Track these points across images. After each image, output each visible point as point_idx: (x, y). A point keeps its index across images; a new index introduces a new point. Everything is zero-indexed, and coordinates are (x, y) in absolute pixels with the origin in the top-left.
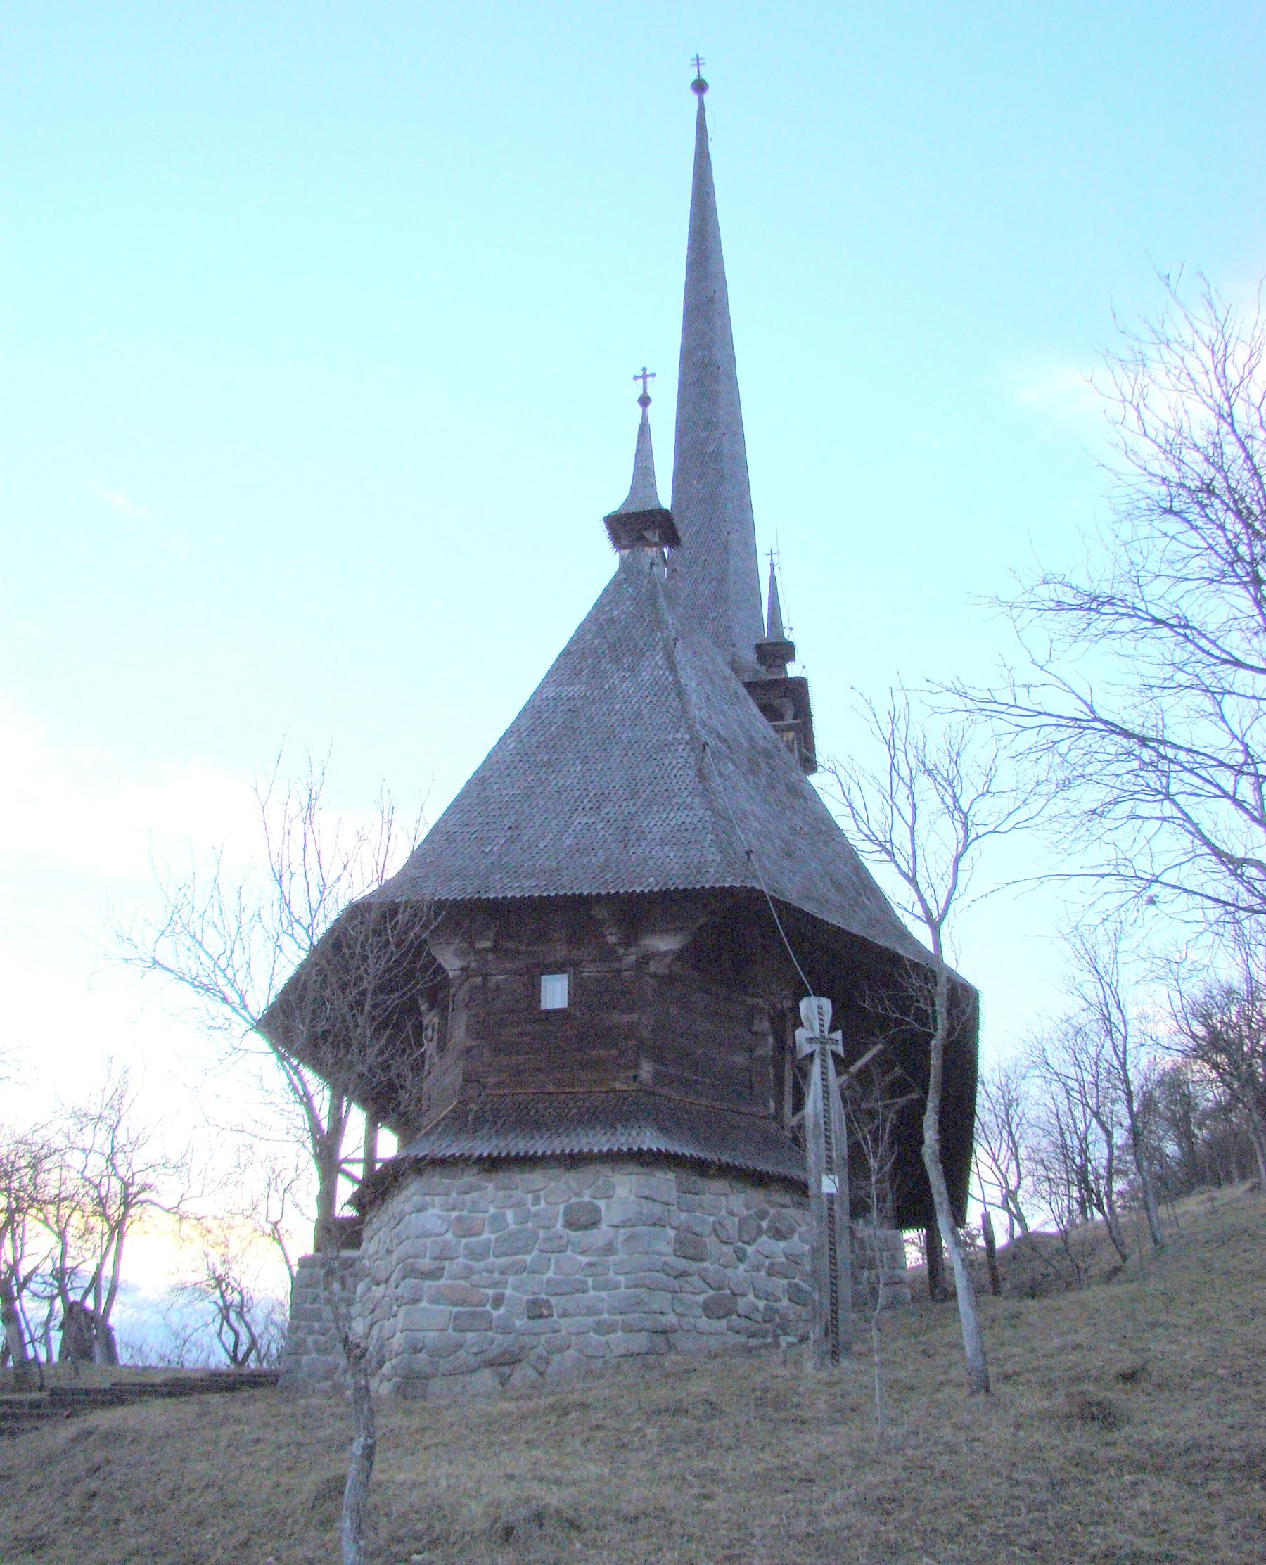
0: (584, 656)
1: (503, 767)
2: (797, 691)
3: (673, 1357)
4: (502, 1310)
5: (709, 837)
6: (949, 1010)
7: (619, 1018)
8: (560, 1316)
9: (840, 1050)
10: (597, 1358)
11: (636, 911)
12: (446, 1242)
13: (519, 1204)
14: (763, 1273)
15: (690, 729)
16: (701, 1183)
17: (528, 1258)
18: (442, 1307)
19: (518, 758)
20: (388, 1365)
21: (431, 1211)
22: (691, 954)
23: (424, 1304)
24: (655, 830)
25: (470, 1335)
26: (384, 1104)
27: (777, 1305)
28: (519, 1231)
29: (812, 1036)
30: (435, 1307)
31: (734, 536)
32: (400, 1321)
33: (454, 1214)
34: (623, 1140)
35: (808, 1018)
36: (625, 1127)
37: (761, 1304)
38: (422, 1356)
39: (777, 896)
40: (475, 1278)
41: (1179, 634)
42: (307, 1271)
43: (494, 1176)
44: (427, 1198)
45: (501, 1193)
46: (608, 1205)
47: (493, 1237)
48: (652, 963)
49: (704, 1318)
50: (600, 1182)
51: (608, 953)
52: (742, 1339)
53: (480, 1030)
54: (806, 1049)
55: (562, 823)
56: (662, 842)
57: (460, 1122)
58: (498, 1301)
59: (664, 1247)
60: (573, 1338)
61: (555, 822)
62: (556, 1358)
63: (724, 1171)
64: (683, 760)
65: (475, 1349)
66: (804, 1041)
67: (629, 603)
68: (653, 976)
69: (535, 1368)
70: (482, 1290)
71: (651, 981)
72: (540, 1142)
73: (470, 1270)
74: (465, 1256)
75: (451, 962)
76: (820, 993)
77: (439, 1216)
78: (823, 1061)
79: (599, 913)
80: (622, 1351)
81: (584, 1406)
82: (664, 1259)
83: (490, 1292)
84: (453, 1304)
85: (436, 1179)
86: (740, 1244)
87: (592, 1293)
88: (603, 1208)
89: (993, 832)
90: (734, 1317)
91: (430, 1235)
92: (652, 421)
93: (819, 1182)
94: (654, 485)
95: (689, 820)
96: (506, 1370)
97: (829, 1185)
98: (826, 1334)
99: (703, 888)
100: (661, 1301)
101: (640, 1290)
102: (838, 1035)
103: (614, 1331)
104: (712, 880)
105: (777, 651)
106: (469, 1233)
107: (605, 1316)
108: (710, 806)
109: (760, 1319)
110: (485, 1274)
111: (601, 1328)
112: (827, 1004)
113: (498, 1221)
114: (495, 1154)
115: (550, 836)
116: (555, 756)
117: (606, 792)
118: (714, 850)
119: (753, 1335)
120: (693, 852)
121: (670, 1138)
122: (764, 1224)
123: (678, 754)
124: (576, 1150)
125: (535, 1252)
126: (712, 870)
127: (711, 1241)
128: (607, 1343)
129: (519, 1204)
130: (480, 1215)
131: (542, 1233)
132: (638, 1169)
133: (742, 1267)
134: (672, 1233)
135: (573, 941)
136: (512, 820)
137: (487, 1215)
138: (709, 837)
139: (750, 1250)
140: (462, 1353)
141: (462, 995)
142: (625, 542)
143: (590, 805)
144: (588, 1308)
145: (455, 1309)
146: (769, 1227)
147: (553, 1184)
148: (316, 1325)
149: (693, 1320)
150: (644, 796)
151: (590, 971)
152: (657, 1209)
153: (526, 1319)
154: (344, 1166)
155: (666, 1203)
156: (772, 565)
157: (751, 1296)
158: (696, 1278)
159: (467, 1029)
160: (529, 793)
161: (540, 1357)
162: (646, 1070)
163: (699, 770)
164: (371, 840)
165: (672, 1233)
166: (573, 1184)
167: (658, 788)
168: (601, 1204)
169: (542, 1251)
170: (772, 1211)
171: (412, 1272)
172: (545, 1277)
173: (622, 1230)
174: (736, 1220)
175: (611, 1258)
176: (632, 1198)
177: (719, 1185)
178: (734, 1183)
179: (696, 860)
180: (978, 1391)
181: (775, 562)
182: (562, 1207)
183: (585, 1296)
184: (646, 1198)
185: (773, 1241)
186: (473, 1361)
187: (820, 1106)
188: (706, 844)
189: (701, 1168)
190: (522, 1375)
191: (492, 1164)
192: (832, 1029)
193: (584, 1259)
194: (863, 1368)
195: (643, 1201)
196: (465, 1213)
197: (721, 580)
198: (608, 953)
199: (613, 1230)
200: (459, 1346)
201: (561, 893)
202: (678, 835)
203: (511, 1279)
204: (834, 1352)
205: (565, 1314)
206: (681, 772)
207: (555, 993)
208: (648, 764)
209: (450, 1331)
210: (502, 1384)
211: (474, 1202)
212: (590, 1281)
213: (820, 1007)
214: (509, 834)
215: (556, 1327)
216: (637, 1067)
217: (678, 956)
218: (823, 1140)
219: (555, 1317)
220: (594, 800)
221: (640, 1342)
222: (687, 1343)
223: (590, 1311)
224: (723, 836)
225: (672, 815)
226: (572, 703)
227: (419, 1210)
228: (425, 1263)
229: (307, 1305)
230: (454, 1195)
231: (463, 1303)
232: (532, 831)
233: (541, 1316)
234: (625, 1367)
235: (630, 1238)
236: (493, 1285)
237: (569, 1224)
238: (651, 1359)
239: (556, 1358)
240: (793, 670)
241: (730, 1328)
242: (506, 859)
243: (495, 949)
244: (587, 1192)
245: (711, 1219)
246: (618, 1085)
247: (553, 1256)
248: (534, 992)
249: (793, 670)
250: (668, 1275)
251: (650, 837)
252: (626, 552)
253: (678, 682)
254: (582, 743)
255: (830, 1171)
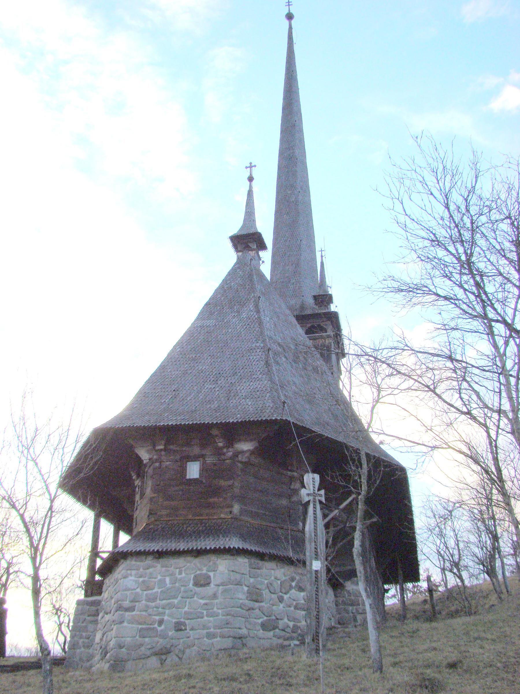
0: (216, 305)
1: (173, 360)
2: (333, 319)
3: (245, 650)
4: (163, 627)
5: (268, 395)
6: (368, 482)
7: (222, 483)
8: (190, 630)
9: (323, 500)
10: (208, 651)
11: (232, 431)
12: (136, 593)
13: (172, 574)
14: (292, 608)
15: (264, 341)
16: (261, 563)
17: (176, 601)
18: (134, 625)
19: (181, 356)
20: (108, 655)
21: (130, 578)
22: (258, 452)
23: (125, 624)
24: (243, 391)
25: (147, 639)
26: (123, 521)
27: (299, 624)
28: (172, 588)
29: (309, 492)
30: (130, 625)
31: (304, 242)
32: (113, 633)
33: (141, 579)
34: (222, 543)
35: (307, 484)
36: (223, 537)
37: (291, 624)
38: (124, 650)
39: (298, 423)
40: (150, 610)
41: (452, 303)
42: (80, 607)
43: (160, 560)
44: (129, 572)
45: (164, 569)
46: (214, 575)
47: (159, 590)
48: (239, 456)
49: (261, 631)
50: (211, 563)
51: (218, 452)
52: (280, 641)
53: (156, 490)
54: (306, 499)
55: (199, 389)
56: (245, 398)
57: (148, 534)
58: (161, 622)
59: (240, 596)
60: (196, 640)
61: (196, 387)
62: (188, 651)
63: (273, 558)
64: (259, 357)
65: (149, 647)
66: (305, 495)
67: (239, 279)
68: (241, 462)
69: (177, 656)
70: (153, 617)
71: (239, 465)
72: (183, 544)
73: (148, 606)
74: (146, 600)
75: (144, 455)
76: (314, 472)
77: (133, 581)
78: (314, 505)
79: (215, 432)
80: (219, 647)
81: (189, 676)
82: (241, 601)
83: (157, 618)
84: (140, 624)
85: (133, 562)
86: (281, 594)
87: (206, 618)
88: (212, 577)
89: (390, 394)
90: (277, 630)
91: (129, 590)
92: (254, 189)
93: (311, 564)
94: (254, 221)
95: (259, 386)
96: (164, 657)
97: (317, 565)
98: (313, 640)
99: (258, 420)
100: (239, 622)
101: (228, 617)
102: (322, 492)
103: (216, 637)
104: (267, 416)
105: (324, 299)
106: (148, 588)
107: (212, 630)
108: (271, 380)
109: (290, 631)
110: (155, 609)
111: (210, 636)
112: (317, 477)
113: (162, 582)
114: (160, 550)
115: (193, 394)
116: (198, 355)
117: (221, 372)
118: (270, 401)
119: (287, 639)
120: (260, 402)
121: (245, 542)
122: (294, 584)
123: (257, 354)
124: (199, 548)
125: (179, 598)
126: (268, 411)
127: (266, 593)
128: (213, 644)
129: (172, 574)
130: (153, 580)
131: (183, 589)
132: (229, 557)
133: (281, 605)
134: (246, 589)
135: (203, 446)
136: (176, 387)
137: (156, 580)
138: (268, 395)
139: (286, 597)
140: (143, 648)
141: (150, 471)
142: (239, 249)
143: (213, 379)
144: (204, 626)
145: (140, 626)
146: (296, 585)
147: (188, 564)
148: (84, 634)
149: (255, 632)
150: (239, 374)
151: (209, 460)
152: (238, 576)
153: (174, 632)
154: (100, 554)
155: (243, 574)
156: (322, 256)
157: (286, 620)
158: (257, 610)
159: (151, 489)
160: (185, 373)
161: (180, 650)
162: (236, 508)
163: (267, 362)
164: (109, 395)
165: (246, 589)
166: (198, 565)
167: (246, 370)
168: (211, 574)
169: (182, 598)
170: (297, 578)
171: (120, 608)
172: (184, 610)
173: (221, 587)
174: (279, 582)
175: (216, 601)
176: (226, 571)
177: (271, 565)
178: (279, 564)
179: (261, 406)
180: (376, 671)
181: (323, 255)
182: (192, 576)
183: (202, 620)
184: (233, 571)
185: (298, 592)
186: (148, 653)
187: (313, 527)
188: (267, 398)
189: (261, 556)
190: (172, 659)
191: (160, 555)
192: (319, 490)
193: (203, 602)
194: (329, 658)
195: (232, 573)
196: (146, 579)
197: (298, 265)
198: (218, 452)
199: (217, 587)
200: (142, 645)
201: (195, 423)
202: (254, 393)
203: (167, 611)
204: (317, 649)
205: (192, 629)
206: (258, 362)
207: (194, 471)
208: (242, 358)
209: (138, 637)
210: (162, 664)
211: (151, 573)
212: (205, 612)
213: (313, 478)
214: (174, 393)
215: (188, 635)
216: (232, 507)
217: (252, 452)
218: (313, 544)
219: (188, 630)
220: (215, 377)
221: (228, 643)
222: (251, 643)
223: (204, 627)
224: (275, 394)
225: (252, 383)
226: (209, 329)
227: (125, 577)
228: (127, 604)
229: (79, 624)
230: (141, 570)
231: (145, 623)
232: (185, 392)
233: (181, 630)
234: (220, 656)
235: (225, 591)
236: (159, 614)
237: (196, 584)
238: (233, 652)
239: (188, 651)
240: (333, 308)
241: (275, 636)
242: (171, 406)
243: (165, 450)
244: (205, 569)
245: (266, 582)
246: (222, 516)
247: (188, 600)
248: (183, 470)
249: (333, 308)
250: (243, 609)
251: (240, 395)
252: (240, 254)
253: (259, 318)
254: (211, 349)
255: (317, 559)
